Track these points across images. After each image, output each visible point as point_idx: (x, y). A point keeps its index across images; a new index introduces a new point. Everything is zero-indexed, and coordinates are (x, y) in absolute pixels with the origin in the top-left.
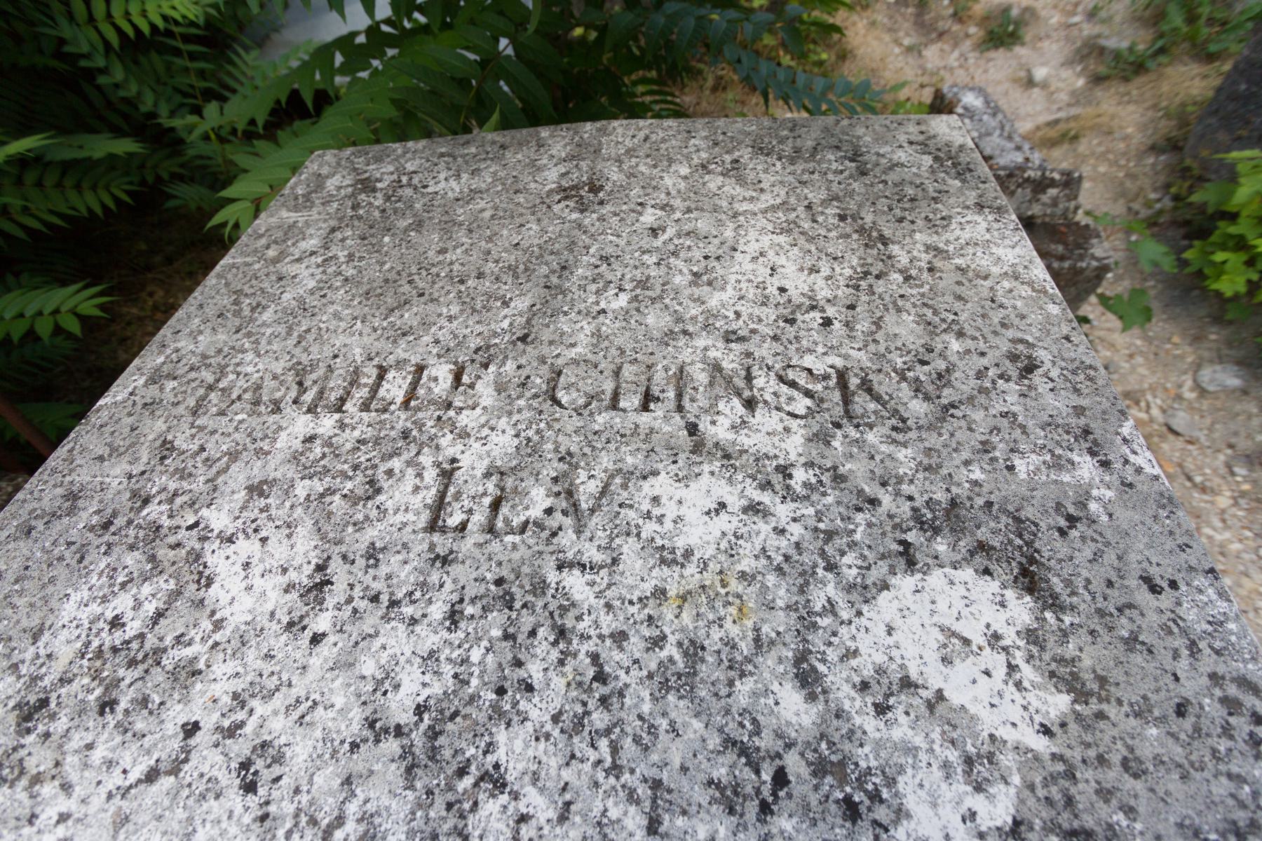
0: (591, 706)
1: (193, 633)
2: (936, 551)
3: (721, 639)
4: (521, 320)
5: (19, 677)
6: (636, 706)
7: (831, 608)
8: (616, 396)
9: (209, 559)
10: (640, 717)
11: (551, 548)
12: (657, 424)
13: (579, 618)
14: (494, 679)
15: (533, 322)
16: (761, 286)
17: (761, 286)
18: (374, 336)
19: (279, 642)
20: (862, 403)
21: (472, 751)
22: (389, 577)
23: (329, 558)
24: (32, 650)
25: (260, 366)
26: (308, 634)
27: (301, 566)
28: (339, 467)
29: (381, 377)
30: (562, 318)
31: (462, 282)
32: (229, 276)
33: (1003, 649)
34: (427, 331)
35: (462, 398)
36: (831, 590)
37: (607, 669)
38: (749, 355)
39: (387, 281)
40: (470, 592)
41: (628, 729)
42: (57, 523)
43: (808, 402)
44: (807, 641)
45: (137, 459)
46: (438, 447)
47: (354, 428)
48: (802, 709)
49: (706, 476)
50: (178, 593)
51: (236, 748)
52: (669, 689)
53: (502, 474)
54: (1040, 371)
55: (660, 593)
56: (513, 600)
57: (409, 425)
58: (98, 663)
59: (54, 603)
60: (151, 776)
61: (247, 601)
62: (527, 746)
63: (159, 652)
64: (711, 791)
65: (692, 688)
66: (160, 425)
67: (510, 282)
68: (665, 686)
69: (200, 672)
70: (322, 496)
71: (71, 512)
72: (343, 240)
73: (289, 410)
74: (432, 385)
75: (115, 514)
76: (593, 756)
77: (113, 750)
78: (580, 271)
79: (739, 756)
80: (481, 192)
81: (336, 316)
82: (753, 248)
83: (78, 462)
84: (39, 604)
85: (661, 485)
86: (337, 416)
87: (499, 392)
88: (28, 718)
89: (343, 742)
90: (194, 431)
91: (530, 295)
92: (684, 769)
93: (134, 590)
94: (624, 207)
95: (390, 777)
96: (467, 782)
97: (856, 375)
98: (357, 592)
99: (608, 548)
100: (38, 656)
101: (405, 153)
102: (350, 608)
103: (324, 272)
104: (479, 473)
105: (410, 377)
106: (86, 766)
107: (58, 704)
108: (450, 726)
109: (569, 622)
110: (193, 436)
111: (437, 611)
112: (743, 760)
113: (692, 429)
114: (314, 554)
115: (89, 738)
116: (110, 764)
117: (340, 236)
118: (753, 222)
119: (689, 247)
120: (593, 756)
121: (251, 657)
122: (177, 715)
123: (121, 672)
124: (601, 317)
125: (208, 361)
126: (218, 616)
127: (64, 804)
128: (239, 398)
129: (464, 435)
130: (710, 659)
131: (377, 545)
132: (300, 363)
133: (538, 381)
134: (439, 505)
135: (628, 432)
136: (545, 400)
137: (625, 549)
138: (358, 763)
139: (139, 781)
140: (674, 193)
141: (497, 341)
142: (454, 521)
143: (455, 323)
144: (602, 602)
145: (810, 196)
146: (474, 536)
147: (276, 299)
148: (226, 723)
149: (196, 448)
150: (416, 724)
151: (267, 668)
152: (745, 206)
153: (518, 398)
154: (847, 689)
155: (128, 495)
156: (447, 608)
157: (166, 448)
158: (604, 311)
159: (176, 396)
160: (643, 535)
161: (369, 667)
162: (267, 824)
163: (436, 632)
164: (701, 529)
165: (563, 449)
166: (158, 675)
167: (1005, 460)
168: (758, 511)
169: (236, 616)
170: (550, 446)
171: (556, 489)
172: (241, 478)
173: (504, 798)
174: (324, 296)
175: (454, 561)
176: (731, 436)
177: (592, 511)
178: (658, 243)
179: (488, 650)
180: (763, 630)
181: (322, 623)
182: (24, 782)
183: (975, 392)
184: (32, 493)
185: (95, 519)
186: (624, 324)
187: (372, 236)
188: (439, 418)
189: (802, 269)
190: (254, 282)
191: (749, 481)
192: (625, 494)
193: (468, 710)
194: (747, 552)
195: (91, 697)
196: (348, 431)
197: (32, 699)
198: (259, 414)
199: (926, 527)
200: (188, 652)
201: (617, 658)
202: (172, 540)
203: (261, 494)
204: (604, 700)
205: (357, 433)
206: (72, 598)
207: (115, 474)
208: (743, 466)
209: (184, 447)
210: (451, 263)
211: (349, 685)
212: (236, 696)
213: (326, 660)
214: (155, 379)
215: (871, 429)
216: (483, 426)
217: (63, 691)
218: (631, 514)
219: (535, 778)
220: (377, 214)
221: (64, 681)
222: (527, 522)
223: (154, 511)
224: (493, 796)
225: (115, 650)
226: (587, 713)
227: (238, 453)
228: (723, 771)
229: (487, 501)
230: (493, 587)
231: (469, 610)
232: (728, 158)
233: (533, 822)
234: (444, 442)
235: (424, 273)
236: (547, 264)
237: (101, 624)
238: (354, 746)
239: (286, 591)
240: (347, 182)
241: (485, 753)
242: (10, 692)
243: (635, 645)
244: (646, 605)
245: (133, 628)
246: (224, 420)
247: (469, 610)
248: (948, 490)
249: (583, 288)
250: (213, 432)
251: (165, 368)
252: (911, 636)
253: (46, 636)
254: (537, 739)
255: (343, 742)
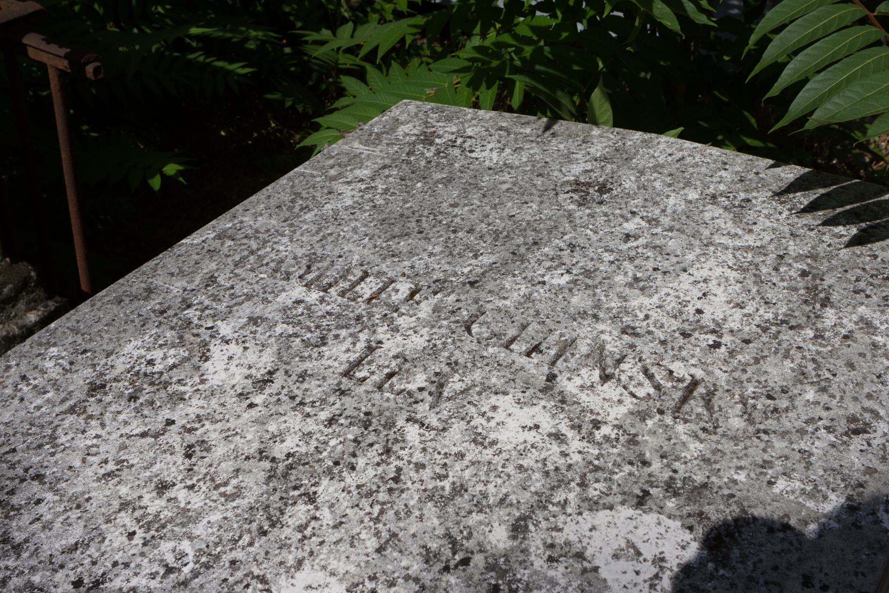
0: (381, 489)
1: (188, 381)
2: (665, 504)
3: (481, 491)
4: (479, 270)
5: (95, 371)
6: (407, 499)
7: (565, 504)
8: (513, 340)
9: (211, 347)
10: (406, 505)
11: (409, 409)
12: (527, 367)
13: (403, 448)
14: (337, 457)
15: (487, 275)
16: (684, 304)
17: (684, 304)
18: (372, 251)
19: (231, 400)
20: (696, 406)
21: (306, 482)
22: (306, 390)
23: (278, 369)
24: (105, 360)
25: (289, 248)
26: (248, 402)
27: (260, 368)
28: (308, 323)
29: (362, 279)
30: (509, 278)
31: (454, 232)
32: (297, 181)
33: (660, 567)
34: (409, 258)
35: (408, 308)
36: (571, 496)
37: (402, 477)
38: (632, 346)
39: (402, 215)
40: (347, 413)
41: (396, 508)
42: (137, 302)
43: (652, 391)
44: (534, 513)
45: (193, 281)
46: (374, 332)
47: (329, 304)
48: (503, 540)
49: (539, 407)
50: (188, 359)
51: (189, 438)
52: (431, 500)
53: (406, 360)
54: (866, 436)
55: (461, 456)
56: (370, 425)
57: (364, 313)
58: (135, 378)
59: (121, 342)
60: (144, 435)
61: (223, 375)
62: (336, 491)
63: (167, 384)
64: (422, 550)
65: (445, 505)
66: (213, 266)
67: (488, 242)
68: (431, 498)
69: (185, 400)
70: (290, 336)
71: (146, 299)
72: (387, 177)
73: (294, 281)
74: (393, 294)
75: (169, 308)
76: (368, 509)
77: (130, 418)
78: (547, 249)
79: (449, 543)
80: (512, 167)
81: (355, 230)
82: (699, 275)
83: (159, 272)
84: (114, 340)
85: (505, 402)
86: (322, 294)
87: (434, 311)
88: (94, 390)
89: (242, 454)
90: (232, 275)
91: (498, 255)
92: (414, 536)
93: (166, 350)
94: (618, 212)
95: (259, 476)
96: (296, 493)
97: (706, 387)
98: (285, 391)
99: (446, 422)
100: (106, 364)
101: (473, 119)
102: (277, 397)
103: (362, 197)
104: (391, 354)
105: (381, 284)
106: (115, 420)
107: (110, 389)
108: (301, 467)
109: (396, 448)
110: (230, 278)
111: (324, 415)
112: (450, 546)
113: (551, 378)
114: (270, 365)
115: (120, 409)
116: (126, 423)
117: (387, 173)
118: (719, 254)
119: (648, 257)
120: (368, 509)
121: (214, 402)
122: (166, 414)
123: (145, 386)
124: (539, 287)
125: (258, 235)
126: (204, 377)
127: (99, 431)
128: (267, 264)
129: (396, 330)
130: (466, 497)
131: (308, 372)
132: (315, 254)
133: (465, 313)
134: (358, 363)
135: (505, 364)
136: (461, 326)
137: (455, 426)
138: (246, 465)
139: (137, 435)
140: (669, 211)
141: (454, 279)
142: (360, 375)
143: (433, 258)
144: (422, 446)
145: (790, 248)
146: (368, 386)
147: (320, 206)
148: (188, 426)
149: (229, 285)
150: (284, 460)
151: (220, 409)
152: (724, 240)
153: (445, 319)
154: (539, 543)
155: (180, 300)
156: (330, 416)
157: (212, 280)
158: (544, 283)
159: (229, 251)
160: (472, 423)
161: (273, 427)
162: (190, 473)
163: (317, 425)
164: (513, 434)
165: (453, 359)
166: (163, 394)
167: (772, 477)
168: (559, 438)
169: (214, 380)
170: (446, 354)
171: (433, 379)
172: (248, 311)
173: (311, 507)
174: (353, 214)
175: (349, 395)
176: (575, 391)
177: (449, 399)
178: (624, 247)
179: (341, 442)
180: (510, 497)
181: (258, 399)
182: (84, 416)
183: (794, 430)
184: (128, 281)
185: (157, 307)
186: (552, 296)
187: (410, 179)
188: (386, 315)
189: (729, 302)
190: (311, 190)
191: (567, 420)
192: (477, 398)
193: (314, 464)
194: (533, 457)
195: (127, 392)
196: (324, 305)
197: (98, 382)
198: (275, 278)
199: (670, 490)
200: (182, 389)
201: (412, 475)
202: (195, 331)
203: (255, 324)
204: (390, 490)
205: (329, 308)
206: (132, 343)
207: (177, 286)
208: (569, 411)
209: (222, 283)
210: (456, 216)
211: (258, 432)
212: (198, 416)
213: (252, 417)
214: (221, 236)
215: (685, 423)
216: (411, 329)
217: (114, 384)
218: (473, 409)
219: (332, 506)
220: (423, 163)
221: (116, 380)
222: (404, 390)
223: (191, 313)
224: (306, 504)
225: (145, 375)
226: (378, 492)
227: (253, 296)
228: (435, 545)
229: (387, 371)
230: (362, 415)
231: (342, 421)
232: (743, 195)
233: (320, 522)
234: (380, 330)
235: (432, 217)
236: (525, 237)
237: (143, 360)
238: (247, 458)
239: (246, 378)
240: (416, 132)
241: (312, 485)
242: (89, 376)
243: (426, 474)
244: (447, 458)
245: (158, 368)
246: (252, 275)
247: (342, 421)
248: (708, 477)
249: (539, 262)
250: (243, 280)
251: (230, 232)
252: (604, 536)
253: (113, 357)
254: (343, 491)
255: (242, 454)
